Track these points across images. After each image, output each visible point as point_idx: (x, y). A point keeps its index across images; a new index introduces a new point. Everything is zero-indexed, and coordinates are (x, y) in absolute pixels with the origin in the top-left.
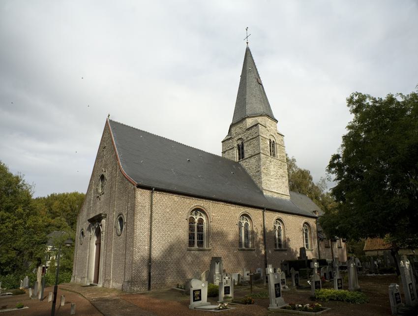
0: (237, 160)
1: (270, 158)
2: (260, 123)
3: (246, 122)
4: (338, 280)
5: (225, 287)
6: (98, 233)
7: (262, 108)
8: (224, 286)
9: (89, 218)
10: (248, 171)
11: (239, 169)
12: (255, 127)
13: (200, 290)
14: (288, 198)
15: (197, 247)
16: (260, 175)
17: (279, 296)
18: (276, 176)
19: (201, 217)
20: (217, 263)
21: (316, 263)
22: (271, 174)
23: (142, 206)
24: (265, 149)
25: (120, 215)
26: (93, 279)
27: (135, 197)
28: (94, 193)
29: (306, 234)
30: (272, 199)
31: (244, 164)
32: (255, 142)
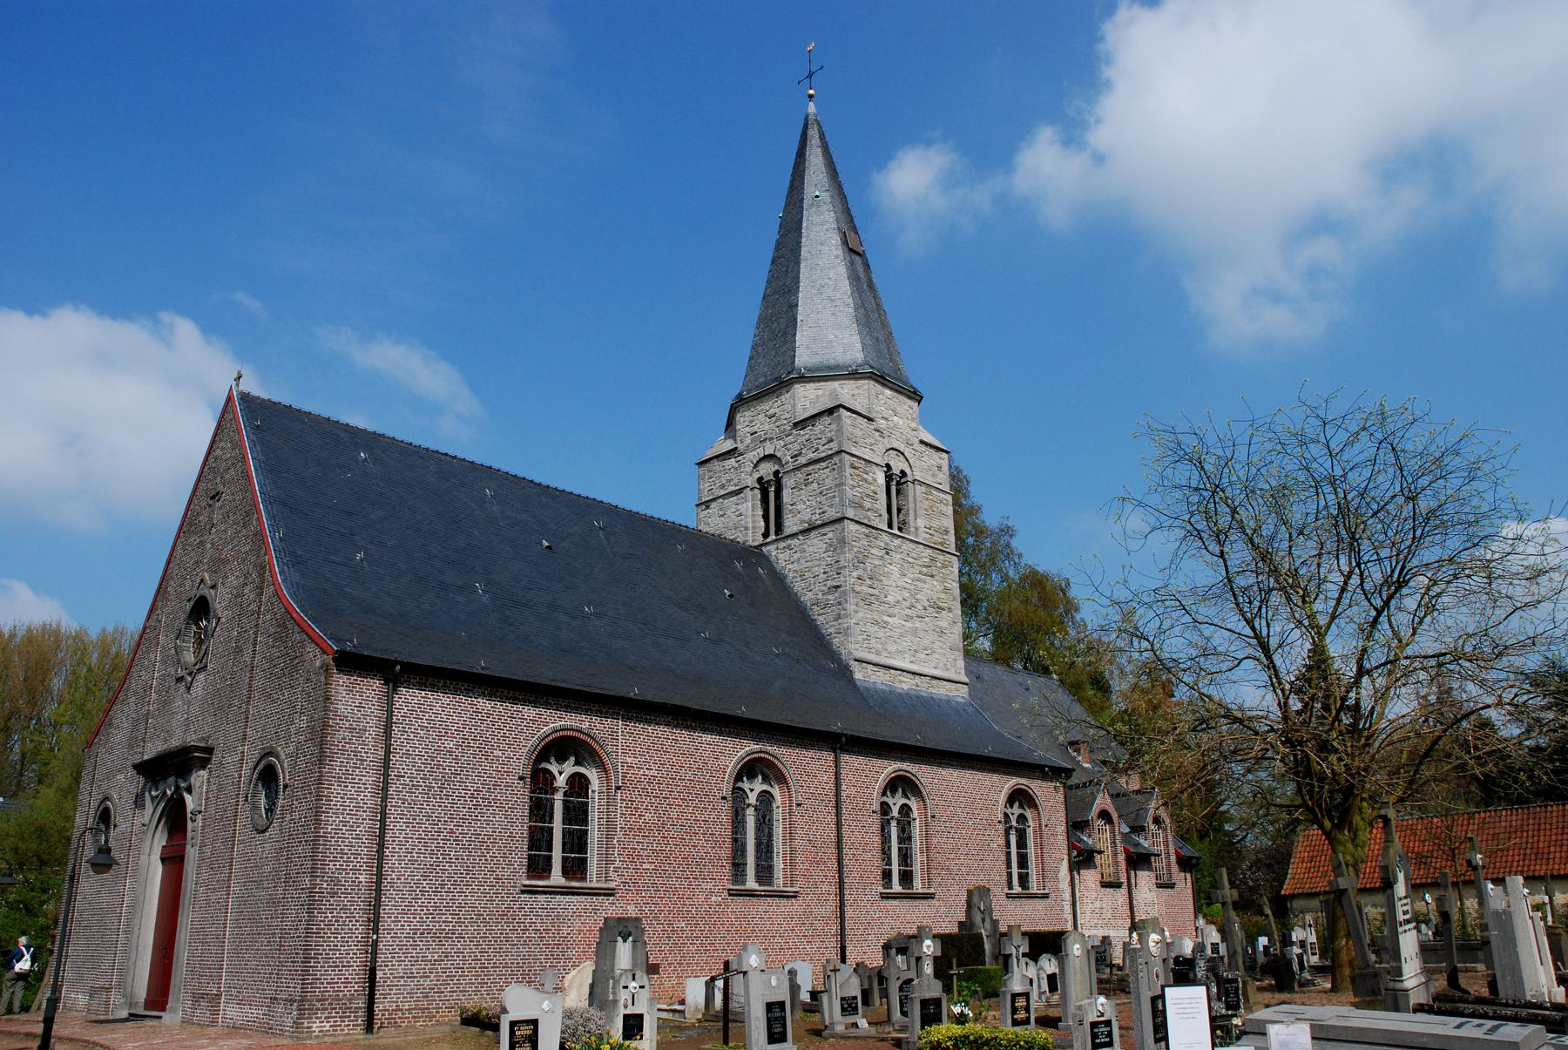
0: (753, 538)
1: (885, 537)
3: (793, 397)
5: (626, 1017)
6: (175, 818)
8: (622, 1011)
9: (138, 759)
10: (798, 587)
11: (757, 578)
12: (826, 420)
13: (535, 1023)
14: (960, 694)
15: (562, 881)
18: (911, 607)
20: (625, 941)
22: (890, 599)
23: (351, 729)
24: (867, 505)
25: (269, 754)
26: (141, 992)
27: (327, 698)
28: (164, 662)
31: (779, 555)
32: (823, 473)
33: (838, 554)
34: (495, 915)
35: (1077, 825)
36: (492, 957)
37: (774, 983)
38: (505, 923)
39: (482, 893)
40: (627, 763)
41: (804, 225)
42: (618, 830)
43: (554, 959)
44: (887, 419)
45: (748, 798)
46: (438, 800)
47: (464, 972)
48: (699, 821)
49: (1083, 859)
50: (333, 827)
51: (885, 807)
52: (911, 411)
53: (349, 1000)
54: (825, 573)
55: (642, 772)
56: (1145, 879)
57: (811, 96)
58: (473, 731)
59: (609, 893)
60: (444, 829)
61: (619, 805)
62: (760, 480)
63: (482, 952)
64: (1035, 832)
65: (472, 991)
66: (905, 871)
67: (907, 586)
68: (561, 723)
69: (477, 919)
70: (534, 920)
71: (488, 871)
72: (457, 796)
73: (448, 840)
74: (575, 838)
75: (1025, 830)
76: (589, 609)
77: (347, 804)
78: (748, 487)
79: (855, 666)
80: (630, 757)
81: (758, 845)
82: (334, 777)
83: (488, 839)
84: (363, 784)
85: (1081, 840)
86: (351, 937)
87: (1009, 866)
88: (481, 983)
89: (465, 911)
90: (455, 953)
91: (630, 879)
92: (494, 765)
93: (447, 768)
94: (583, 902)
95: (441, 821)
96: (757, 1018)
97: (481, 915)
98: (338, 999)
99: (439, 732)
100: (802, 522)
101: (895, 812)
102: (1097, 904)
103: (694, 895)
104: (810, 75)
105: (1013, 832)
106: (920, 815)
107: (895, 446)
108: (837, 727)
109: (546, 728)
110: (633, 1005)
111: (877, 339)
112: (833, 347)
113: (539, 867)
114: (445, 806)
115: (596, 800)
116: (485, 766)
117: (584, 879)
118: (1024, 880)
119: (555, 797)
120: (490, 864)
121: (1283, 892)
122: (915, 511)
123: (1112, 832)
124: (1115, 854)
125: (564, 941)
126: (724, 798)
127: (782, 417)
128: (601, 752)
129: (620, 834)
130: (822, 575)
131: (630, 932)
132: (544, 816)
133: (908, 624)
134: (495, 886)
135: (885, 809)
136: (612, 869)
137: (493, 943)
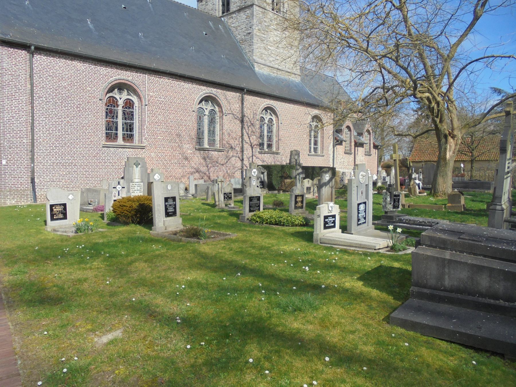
1: (271, 14)
4: (296, 196)
11: (218, 29)
13: (65, 205)
14: (297, 79)
16: (252, 38)
17: (174, 214)
19: (130, 97)
20: (137, 167)
21: (255, 170)
30: (268, 78)
35: (338, 131)
49: (338, 142)
50: (7, 118)
51: (263, 119)
53: (23, 191)
56: (361, 150)
59: (143, 148)
67: (278, 35)
77: (13, 108)
79: (256, 65)
81: (209, 131)
82: (5, 96)
84: (21, 100)
85: (338, 136)
86: (22, 166)
87: (310, 144)
98: (17, 190)
101: (266, 121)
102: (342, 160)
105: (313, 131)
106: (276, 122)
109: (111, 79)
110: (119, 195)
113: (111, 136)
115: (137, 110)
117: (133, 142)
118: (315, 150)
119: (118, 108)
123: (351, 134)
124: (351, 142)
126: (193, 111)
128: (138, 90)
129: (147, 124)
130: (244, 29)
132: (113, 116)
135: (262, 119)
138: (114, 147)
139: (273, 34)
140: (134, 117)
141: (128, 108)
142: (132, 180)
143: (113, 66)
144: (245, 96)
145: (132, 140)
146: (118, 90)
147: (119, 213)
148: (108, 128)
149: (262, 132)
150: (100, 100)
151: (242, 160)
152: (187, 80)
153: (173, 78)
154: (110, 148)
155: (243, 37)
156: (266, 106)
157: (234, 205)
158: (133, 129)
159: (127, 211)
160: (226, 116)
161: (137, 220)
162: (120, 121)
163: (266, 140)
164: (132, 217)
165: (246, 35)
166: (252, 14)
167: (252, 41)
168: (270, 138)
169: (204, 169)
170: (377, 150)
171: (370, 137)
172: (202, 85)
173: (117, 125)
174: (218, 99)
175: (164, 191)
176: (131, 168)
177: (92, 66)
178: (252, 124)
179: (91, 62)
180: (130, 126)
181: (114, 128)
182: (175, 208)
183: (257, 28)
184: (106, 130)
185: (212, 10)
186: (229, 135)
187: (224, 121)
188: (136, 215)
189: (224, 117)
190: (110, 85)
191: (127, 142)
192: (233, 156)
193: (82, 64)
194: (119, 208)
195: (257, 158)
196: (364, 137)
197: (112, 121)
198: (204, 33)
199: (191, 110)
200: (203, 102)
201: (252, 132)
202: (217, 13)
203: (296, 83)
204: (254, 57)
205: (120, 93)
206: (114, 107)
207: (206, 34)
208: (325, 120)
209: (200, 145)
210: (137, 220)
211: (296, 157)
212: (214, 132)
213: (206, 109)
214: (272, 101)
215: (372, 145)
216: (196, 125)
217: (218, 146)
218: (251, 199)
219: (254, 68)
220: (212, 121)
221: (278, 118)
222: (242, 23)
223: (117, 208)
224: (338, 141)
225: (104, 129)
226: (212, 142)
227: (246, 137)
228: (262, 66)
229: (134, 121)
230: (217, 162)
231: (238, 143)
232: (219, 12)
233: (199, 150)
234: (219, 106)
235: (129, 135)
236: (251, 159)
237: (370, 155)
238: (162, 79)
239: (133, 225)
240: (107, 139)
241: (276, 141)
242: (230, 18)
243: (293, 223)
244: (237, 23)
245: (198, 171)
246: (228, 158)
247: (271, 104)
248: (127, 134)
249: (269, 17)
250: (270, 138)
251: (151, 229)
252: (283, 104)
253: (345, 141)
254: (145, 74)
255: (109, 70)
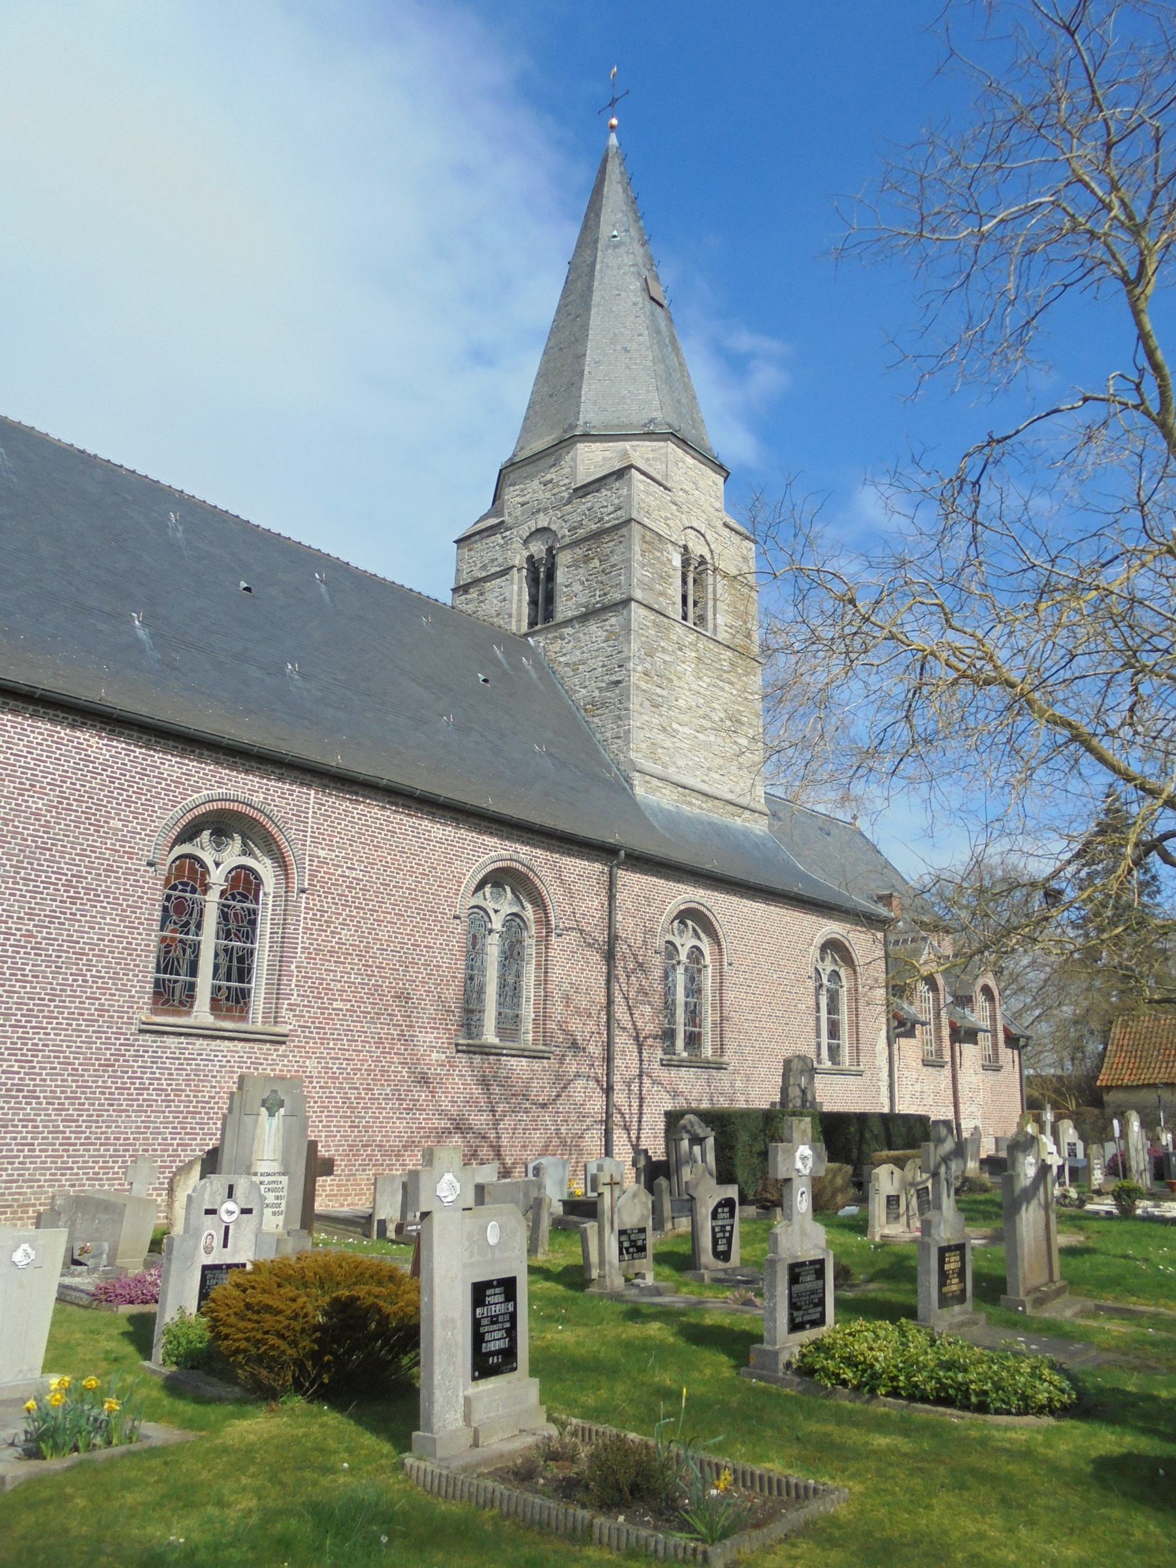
1: (679, 629)
2: (639, 463)
3: (574, 460)
4: (943, 1251)
7: (656, 403)
11: (518, 667)
14: (759, 827)
16: (625, 697)
19: (250, 862)
20: (271, 1115)
22: (681, 703)
29: (833, 997)
30: (673, 820)
33: (621, 643)
34: (94, 1065)
35: (897, 990)
36: (83, 1129)
37: (493, 1238)
38: (109, 1077)
39: (73, 1030)
40: (319, 857)
41: (598, 267)
42: (299, 950)
43: (186, 1134)
44: (686, 492)
45: (491, 921)
46: (10, 885)
47: (34, 1150)
48: (419, 946)
49: (902, 1027)
52: (714, 488)
54: (603, 666)
55: (339, 872)
56: (970, 1053)
57: (612, 127)
58: (78, 787)
59: (279, 1040)
60: (17, 929)
61: (302, 915)
62: (531, 557)
63: (67, 1121)
64: (849, 991)
65: (46, 1181)
66: (691, 1033)
67: (702, 691)
68: (220, 791)
69: (61, 1069)
70: (157, 1075)
71: (88, 998)
72: (42, 882)
73: (22, 947)
74: (235, 960)
75: (837, 991)
76: (293, 666)
78: (514, 566)
79: (637, 779)
80: (323, 849)
81: (503, 985)
83: (90, 949)
88: (61, 1168)
89: (43, 1057)
90: (20, 1120)
91: (313, 1023)
92: (109, 841)
93: (30, 838)
94: (237, 1052)
95: (12, 917)
96: (450, 1323)
97: (69, 1064)
99: (21, 783)
100: (578, 606)
101: (683, 957)
102: (918, 1087)
103: (406, 1050)
104: (614, 101)
105: (824, 992)
107: (695, 525)
108: (613, 838)
109: (196, 795)
110: (225, 1246)
111: (679, 401)
112: (625, 403)
114: (21, 896)
115: (270, 907)
116: (94, 841)
117: (244, 1019)
120: (91, 987)
121: (1098, 1083)
122: (715, 606)
124: (938, 1028)
125: (203, 1108)
126: (456, 917)
127: (561, 483)
128: (280, 838)
129: (300, 956)
130: (600, 670)
131: (283, 1101)
132: (187, 924)
133: (701, 737)
134: (97, 1021)
136: (285, 1006)
137: (86, 1106)
138: (181, 1034)
139: (686, 686)
140: (258, 932)
141: (239, 897)
142: (249, 1167)
143: (206, 753)
144: (620, 873)
145: (242, 1011)
146: (211, 835)
147: (243, 1345)
148: (166, 964)
149: (669, 991)
150: (150, 864)
151: (609, 1090)
152: (440, 812)
153: (396, 805)
154: (165, 1038)
155: (596, 693)
156: (682, 907)
157: (657, 1275)
158: (249, 970)
159: (282, 1337)
160: (560, 935)
161: (319, 1375)
162: (208, 940)
163: (682, 1021)
164: (299, 1364)
165: (607, 689)
166: (627, 627)
167: (626, 705)
168: (693, 1014)
169: (480, 1120)
170: (1016, 1052)
171: (993, 1010)
172: (485, 833)
173: (197, 956)
174: (537, 881)
175: (472, 1253)
176: (248, 1120)
177: (138, 750)
178: (641, 965)
179: (136, 735)
180: (241, 960)
181: (184, 968)
182: (511, 1332)
183: (639, 668)
184: (158, 971)
185: (498, 615)
186: (567, 999)
187: (552, 953)
188: (315, 1356)
189: (553, 938)
190: (189, 816)
191: (224, 1018)
192: (578, 1075)
193: (105, 742)
194: (243, 1319)
195: (654, 1082)
196: (977, 1008)
197: (181, 941)
198: (481, 677)
199: (450, 914)
200: (488, 889)
201: (641, 990)
202: (514, 623)
203: (757, 836)
204: (633, 755)
205: (219, 846)
206: (194, 891)
207: (485, 681)
208: (859, 956)
209: (469, 1035)
210: (319, 1375)
211: (803, 1081)
212: (516, 990)
213: (496, 911)
214: (701, 892)
215: (1001, 1036)
216: (461, 965)
217: (528, 1037)
218: (795, 1272)
219: (632, 786)
220: (512, 954)
221: (719, 944)
222: (594, 654)
223: (232, 1320)
224: (902, 1023)
225: (152, 966)
226: (509, 1024)
227: (620, 1012)
228: (656, 782)
229: (257, 945)
230: (526, 1097)
231: (595, 1028)
232: (519, 621)
233: (470, 1051)
234: (538, 902)
235: (233, 992)
236: (635, 1087)
237: (998, 1069)
238: (361, 807)
239: (298, 1402)
240: (155, 1002)
241: (714, 1023)
242: (556, 637)
243: (1024, 1398)
244: (578, 653)
245: (460, 1127)
246: (563, 1083)
247: (697, 899)
248: (229, 988)
249: (675, 638)
250: (693, 1012)
251: (403, 1443)
252: (735, 900)
253: (923, 1024)
254: (309, 786)
255: (192, 765)
